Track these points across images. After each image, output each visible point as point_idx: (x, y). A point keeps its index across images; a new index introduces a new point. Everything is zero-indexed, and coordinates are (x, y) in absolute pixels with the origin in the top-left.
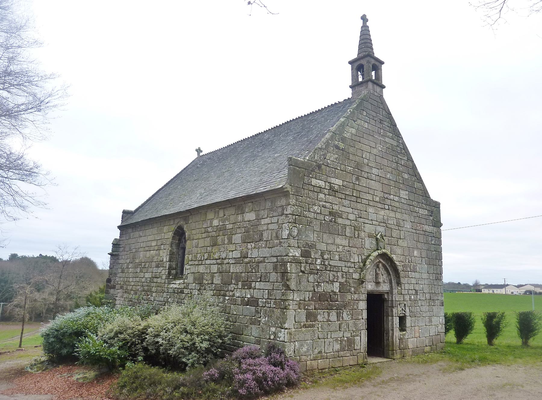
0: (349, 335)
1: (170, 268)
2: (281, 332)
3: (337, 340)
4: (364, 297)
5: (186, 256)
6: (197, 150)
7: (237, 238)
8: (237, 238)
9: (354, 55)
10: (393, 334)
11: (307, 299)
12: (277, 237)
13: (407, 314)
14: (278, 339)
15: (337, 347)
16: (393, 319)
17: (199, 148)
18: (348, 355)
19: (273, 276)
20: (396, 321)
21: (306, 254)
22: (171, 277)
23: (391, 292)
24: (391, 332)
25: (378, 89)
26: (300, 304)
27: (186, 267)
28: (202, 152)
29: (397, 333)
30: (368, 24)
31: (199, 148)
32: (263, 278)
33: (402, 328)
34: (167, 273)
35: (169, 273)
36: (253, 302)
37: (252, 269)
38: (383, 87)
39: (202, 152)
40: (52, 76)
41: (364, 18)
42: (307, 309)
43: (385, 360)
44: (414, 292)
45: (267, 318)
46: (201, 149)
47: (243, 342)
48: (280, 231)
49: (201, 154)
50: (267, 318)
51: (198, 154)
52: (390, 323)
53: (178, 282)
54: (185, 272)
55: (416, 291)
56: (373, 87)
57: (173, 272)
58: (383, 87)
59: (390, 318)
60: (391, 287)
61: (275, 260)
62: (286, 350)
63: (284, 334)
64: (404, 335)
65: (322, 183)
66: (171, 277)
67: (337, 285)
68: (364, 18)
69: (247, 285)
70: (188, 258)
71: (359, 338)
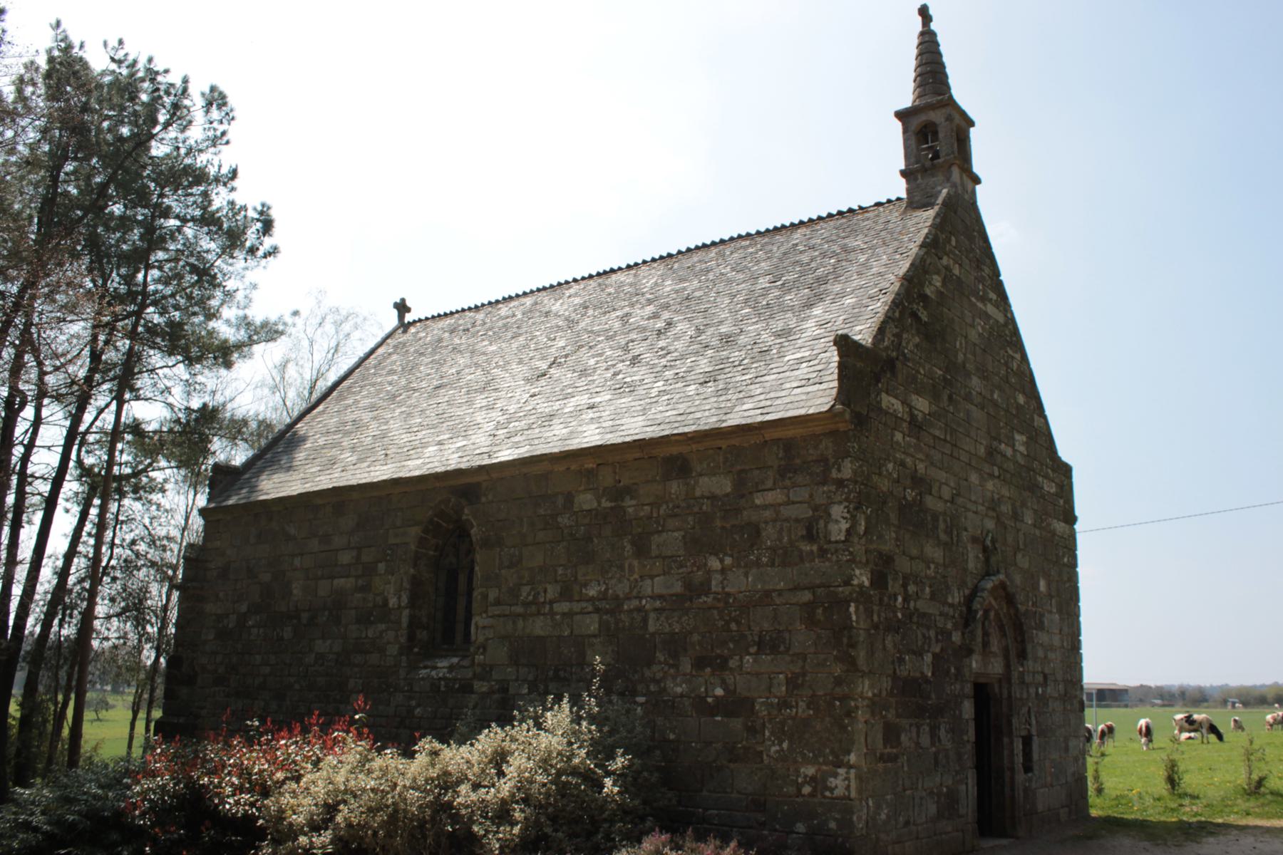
0: (950, 782)
1: (414, 624)
2: (835, 775)
3: (931, 793)
4: (969, 689)
5: (476, 594)
6: (396, 306)
7: (671, 540)
8: (671, 540)
9: (906, 99)
10: (1012, 779)
11: (884, 693)
12: (810, 536)
13: (1034, 732)
14: (828, 794)
15: (933, 809)
16: (1012, 743)
17: (403, 300)
18: (950, 829)
19: (802, 638)
20: (1018, 746)
21: (879, 580)
22: (416, 650)
23: (1006, 678)
24: (1008, 774)
25: (969, 184)
26: (875, 705)
27: (477, 620)
28: (409, 310)
29: (1020, 777)
30: (933, 26)
31: (403, 300)
32: (771, 644)
33: (1028, 768)
34: (403, 640)
35: (411, 638)
36: (736, 705)
37: (728, 623)
38: (977, 180)
39: (409, 310)
40: (166, 71)
41: (924, 12)
42: (884, 717)
43: (1004, 842)
44: (1040, 678)
45: (785, 745)
46: (408, 304)
47: (706, 809)
48: (822, 523)
49: (409, 318)
50: (785, 745)
51: (401, 317)
52: (1006, 752)
53: (442, 663)
54: (477, 636)
55: (1045, 677)
56: (961, 178)
57: (422, 635)
58: (977, 180)
59: (1006, 740)
60: (1008, 666)
61: (807, 596)
62: (855, 818)
63: (847, 779)
64: (1030, 780)
65: (897, 405)
66: (416, 650)
67: (928, 658)
68: (924, 12)
69: (712, 662)
70: (485, 597)
71: (964, 787)
